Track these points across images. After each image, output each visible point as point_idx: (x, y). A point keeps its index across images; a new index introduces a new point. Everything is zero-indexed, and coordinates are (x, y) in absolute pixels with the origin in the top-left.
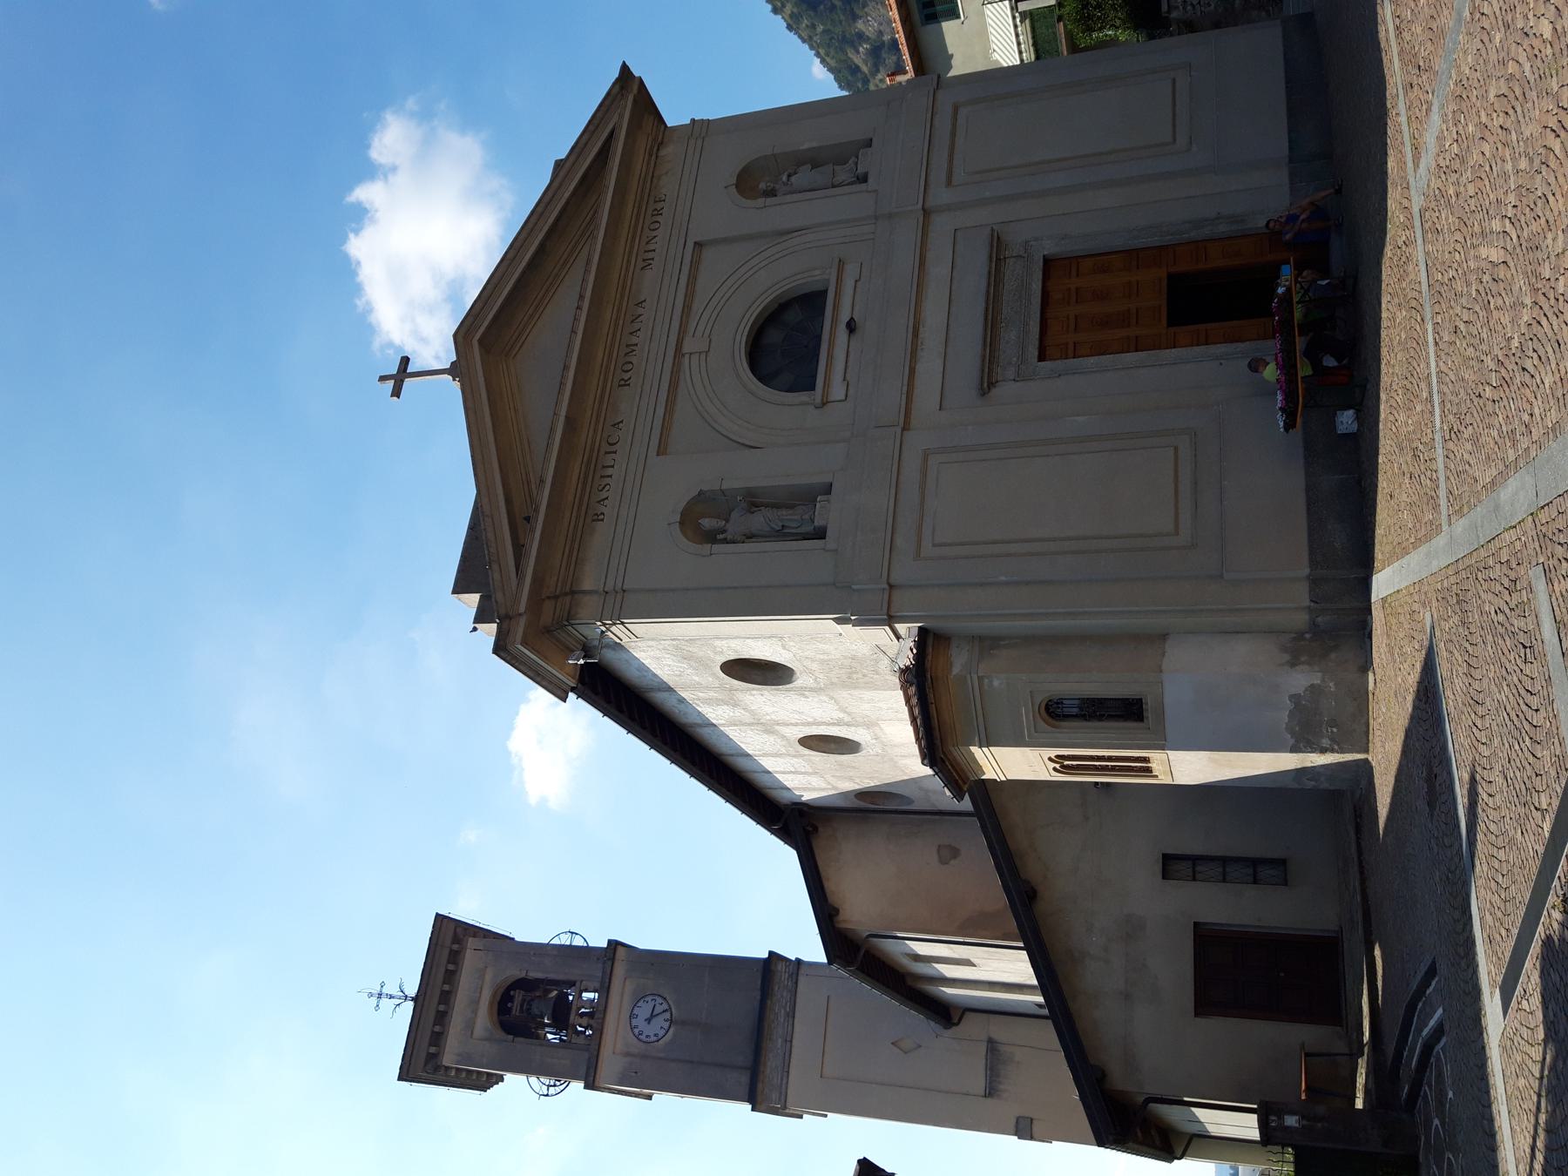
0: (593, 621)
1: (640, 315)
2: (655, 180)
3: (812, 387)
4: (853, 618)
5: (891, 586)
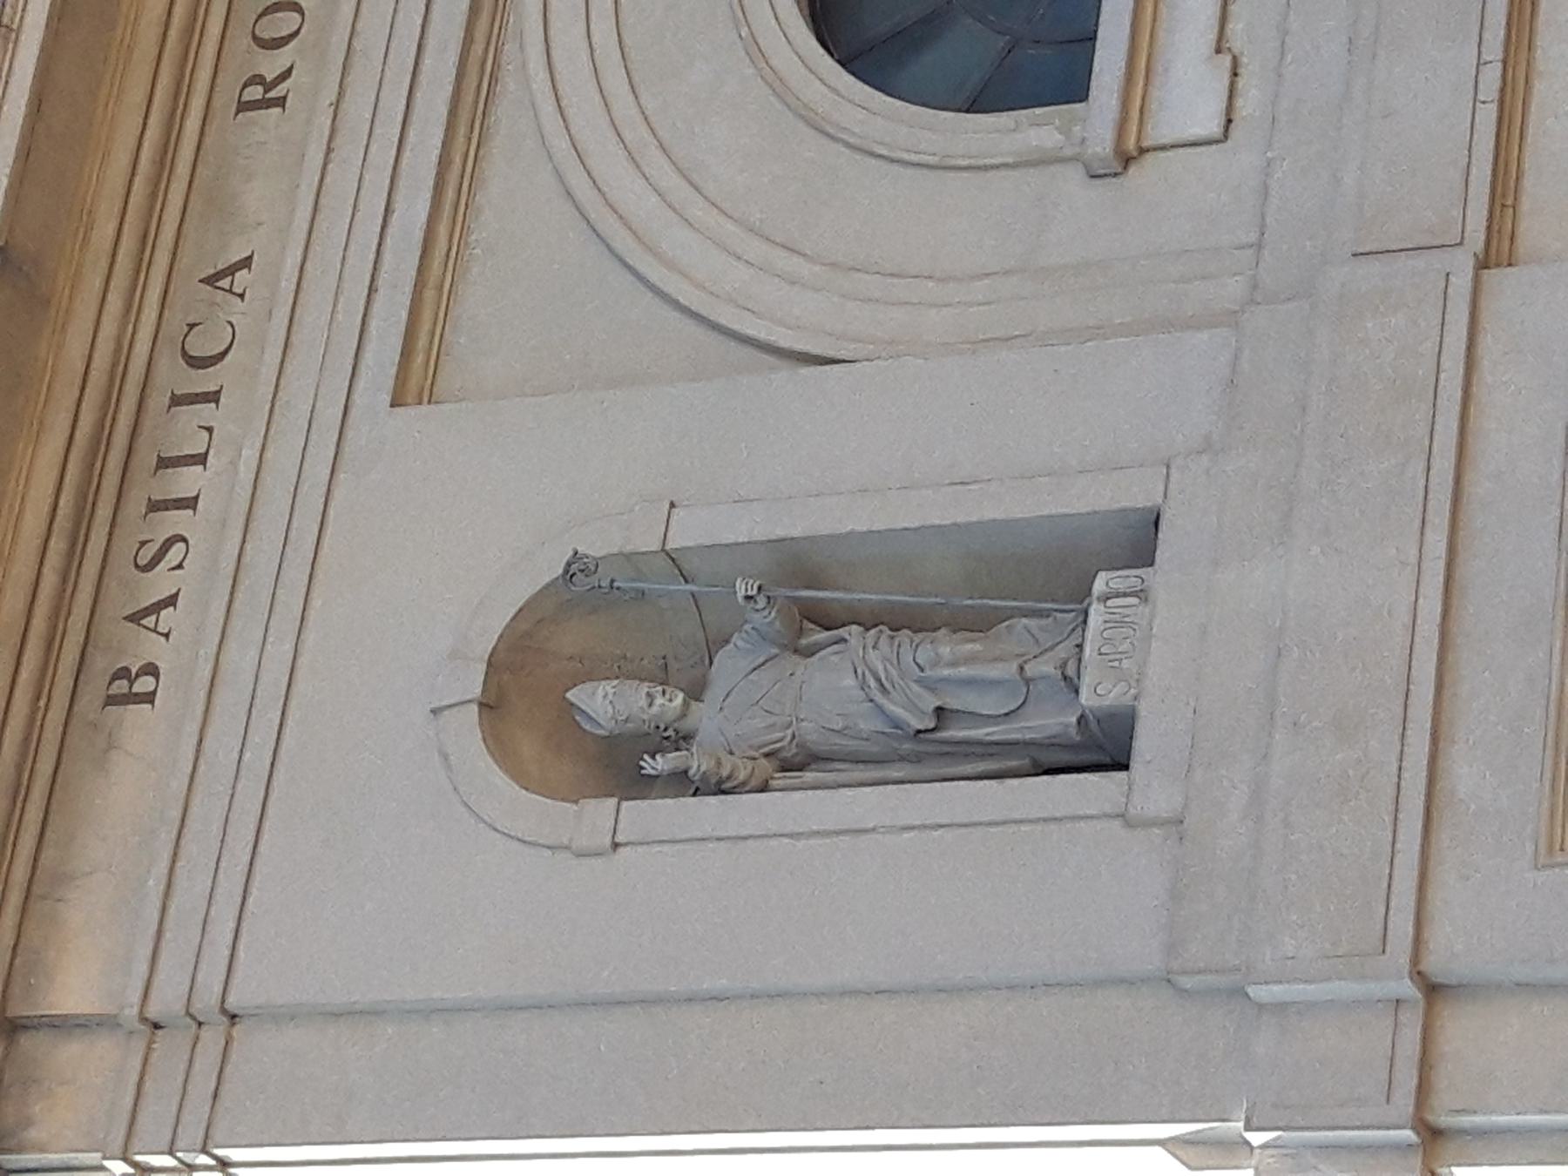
0: (93, 1158)
3: (1074, 88)
4: (1256, 1138)
5: (1433, 990)
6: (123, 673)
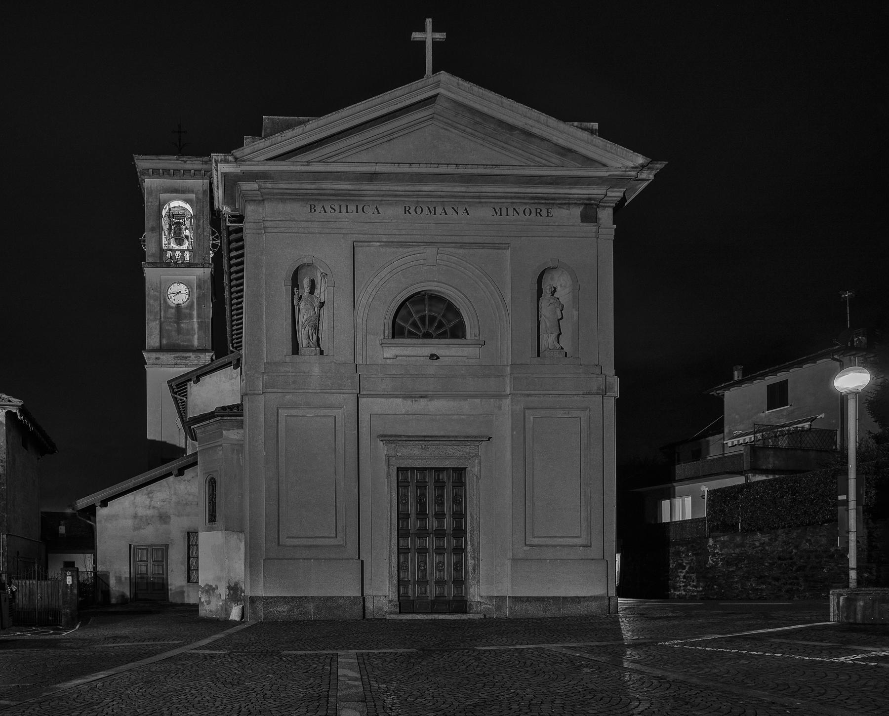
1: (457, 213)
6: (315, 206)
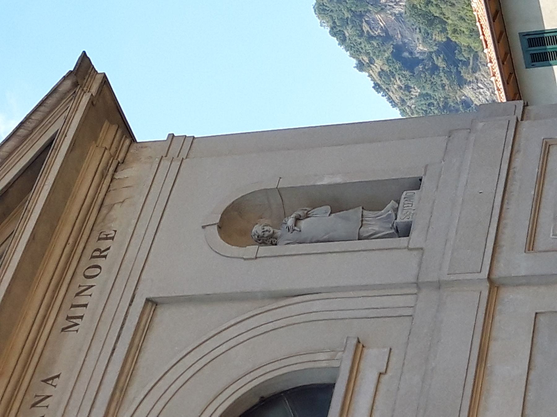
1: (48, 397)
2: (104, 211)
